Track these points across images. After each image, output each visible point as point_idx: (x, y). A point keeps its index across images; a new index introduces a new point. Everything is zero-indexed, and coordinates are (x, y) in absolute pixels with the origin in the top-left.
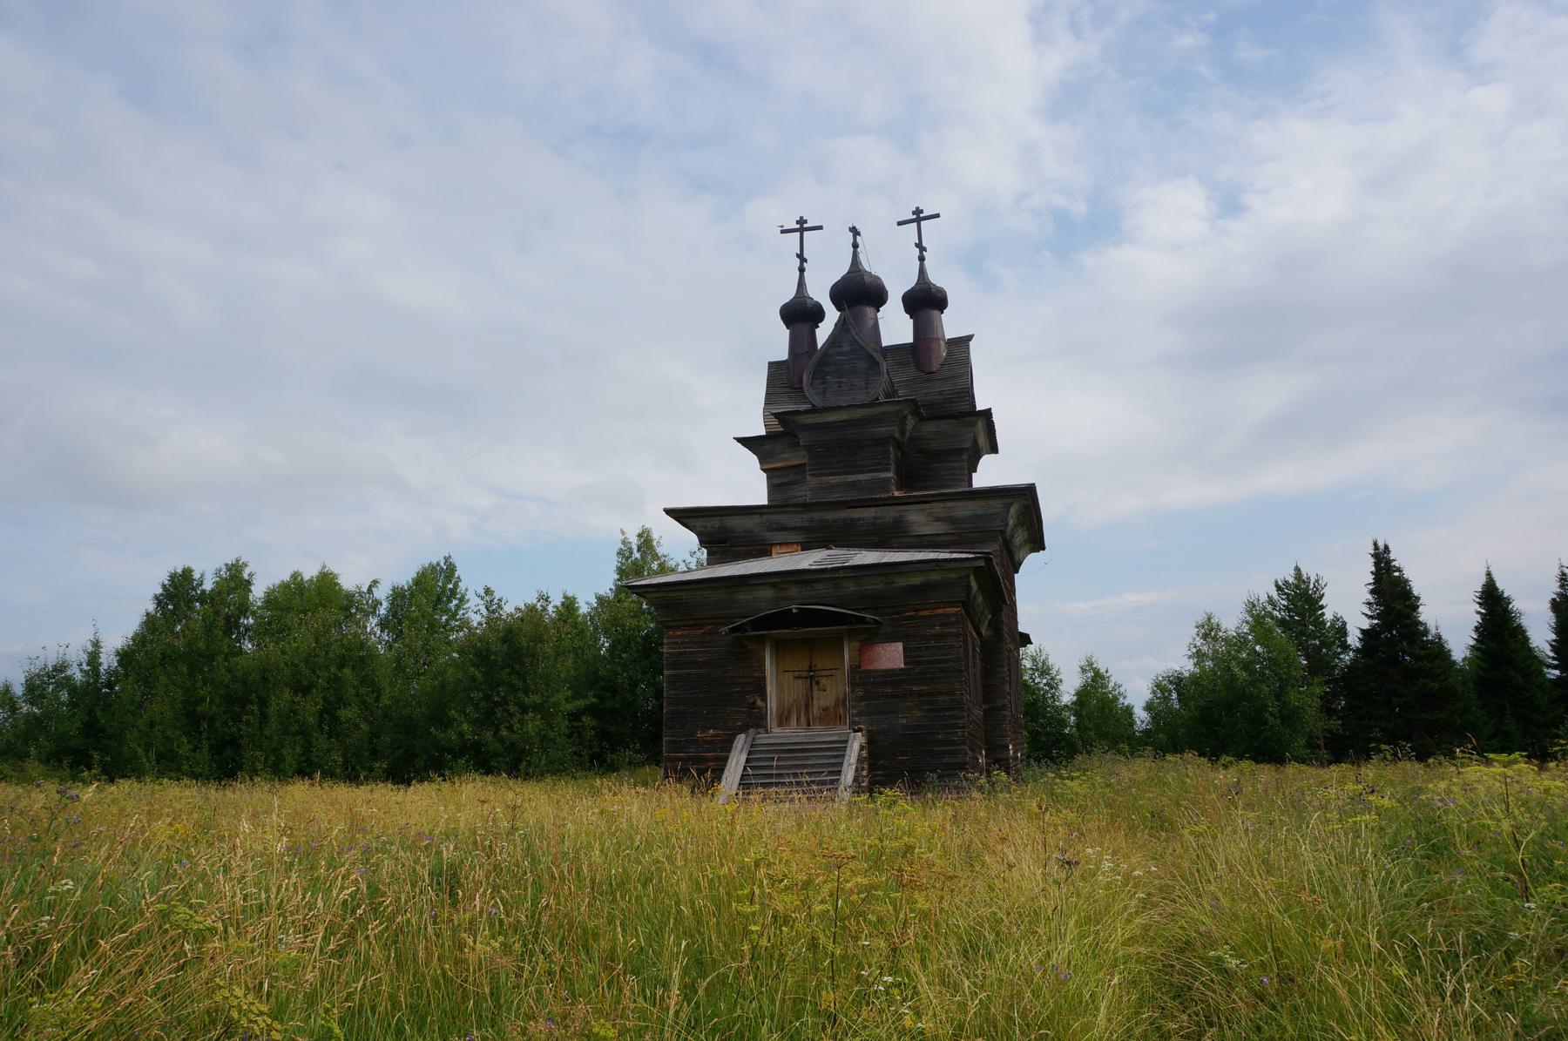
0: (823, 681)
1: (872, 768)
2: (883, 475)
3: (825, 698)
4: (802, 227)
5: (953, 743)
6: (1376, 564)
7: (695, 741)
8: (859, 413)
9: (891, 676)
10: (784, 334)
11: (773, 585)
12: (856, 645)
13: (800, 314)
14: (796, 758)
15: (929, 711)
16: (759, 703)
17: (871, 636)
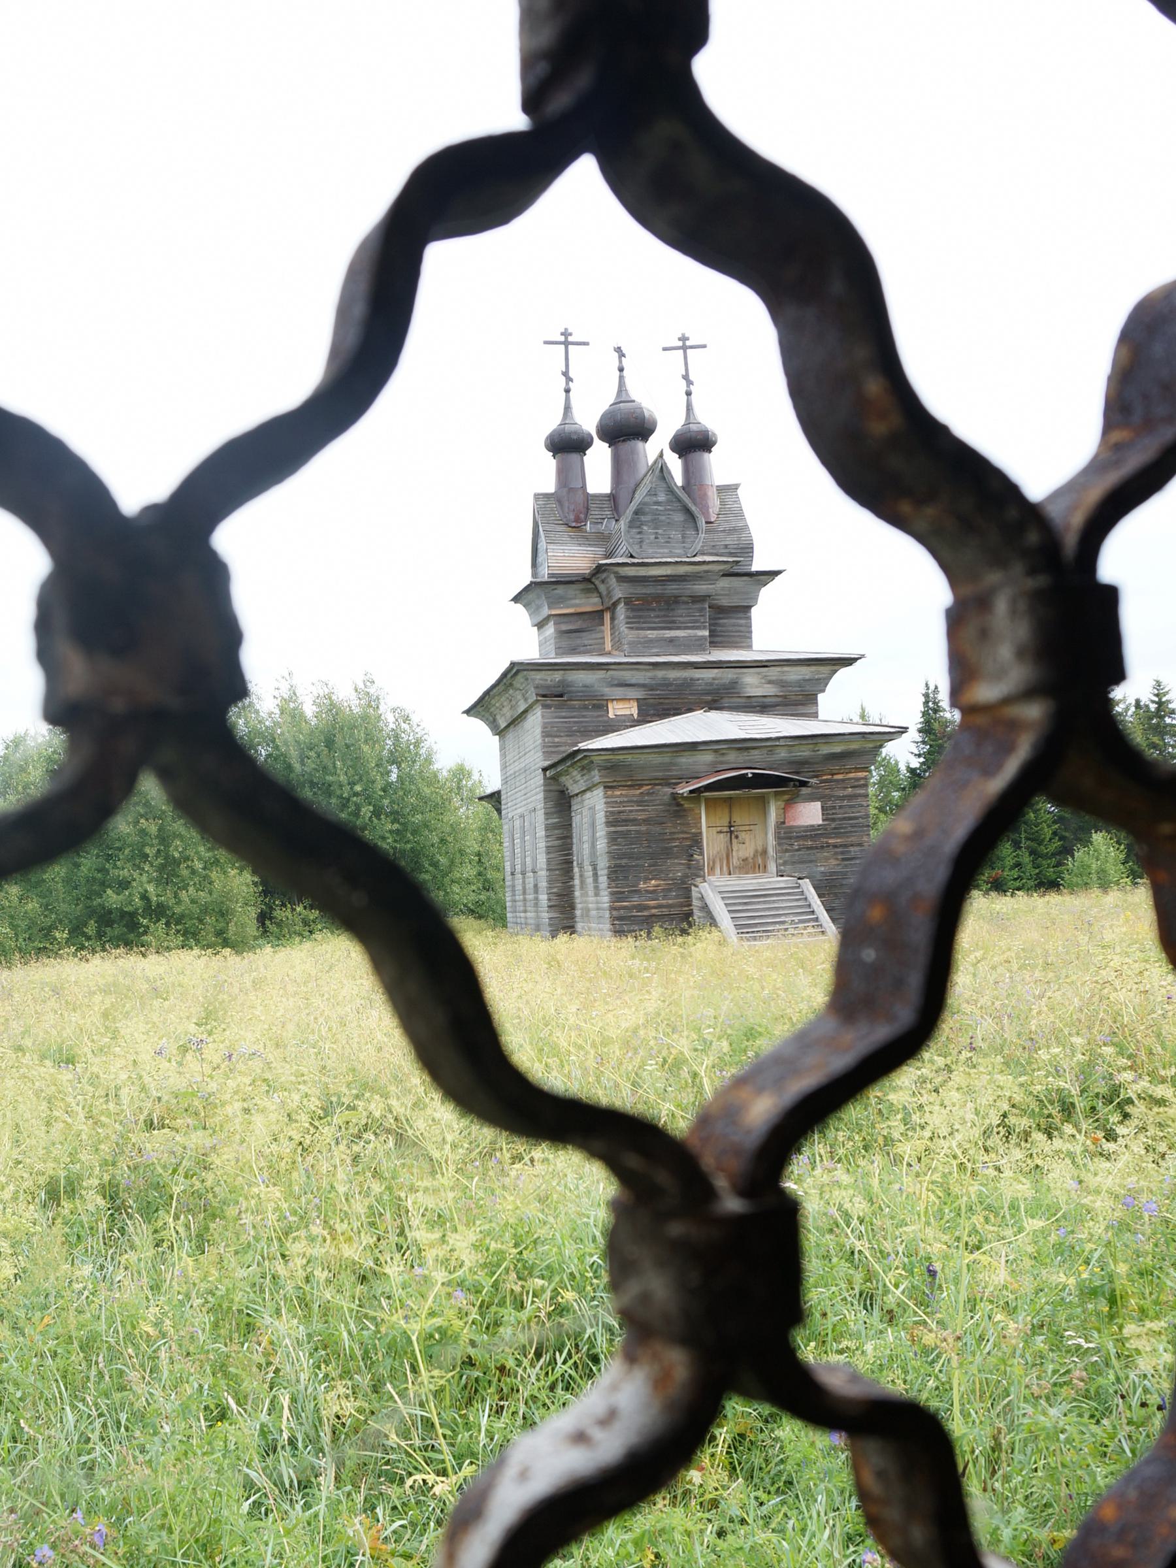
0: (742, 835)
3: (745, 849)
6: (926, 703)
7: (638, 892)
8: (682, 570)
9: (812, 833)
11: (716, 751)
12: (781, 804)
13: (567, 446)
14: (765, 902)
15: (843, 859)
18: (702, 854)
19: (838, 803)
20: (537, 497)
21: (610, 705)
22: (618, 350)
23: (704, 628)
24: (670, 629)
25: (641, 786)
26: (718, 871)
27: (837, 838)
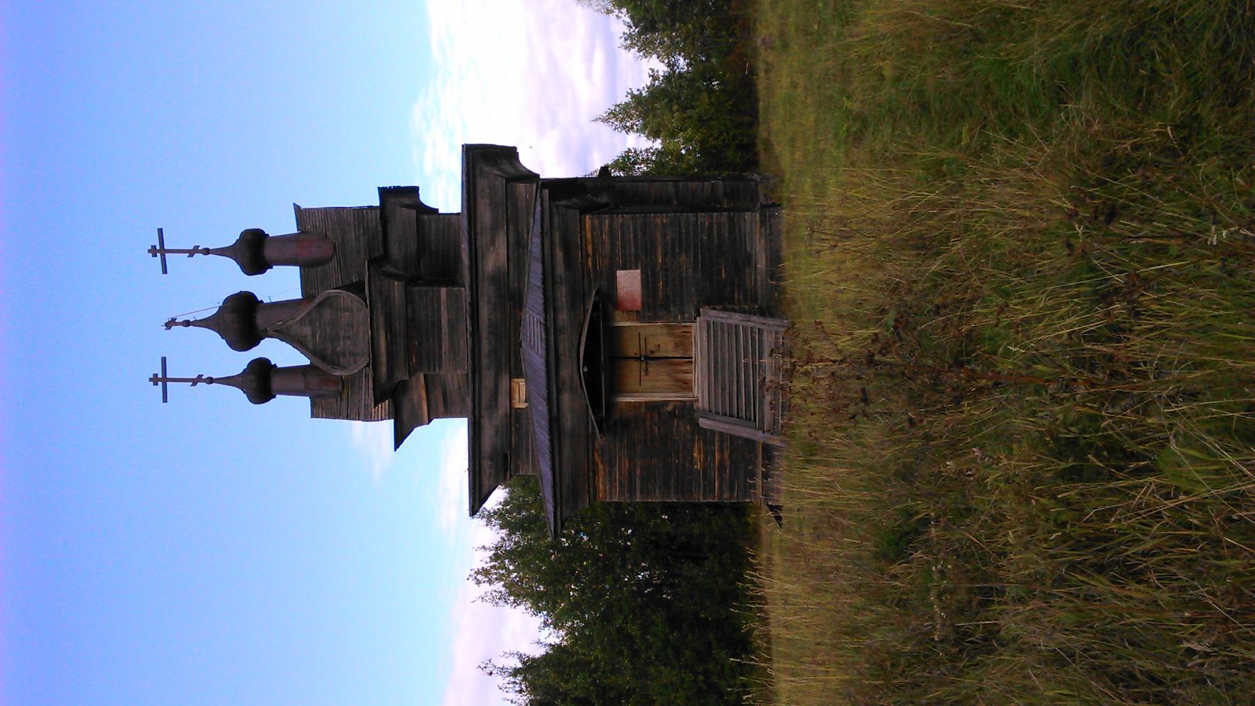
0: (651, 347)
1: (731, 300)
2: (443, 297)
4: (161, 380)
5: (711, 226)
8: (381, 320)
9: (648, 283)
10: (281, 402)
11: (559, 391)
13: (261, 383)
16: (670, 408)
17: (608, 300)
18: (666, 403)
19: (619, 250)
20: (314, 415)
21: (517, 406)
22: (170, 324)
23: (439, 292)
24: (440, 328)
25: (595, 463)
26: (687, 376)
27: (656, 251)
